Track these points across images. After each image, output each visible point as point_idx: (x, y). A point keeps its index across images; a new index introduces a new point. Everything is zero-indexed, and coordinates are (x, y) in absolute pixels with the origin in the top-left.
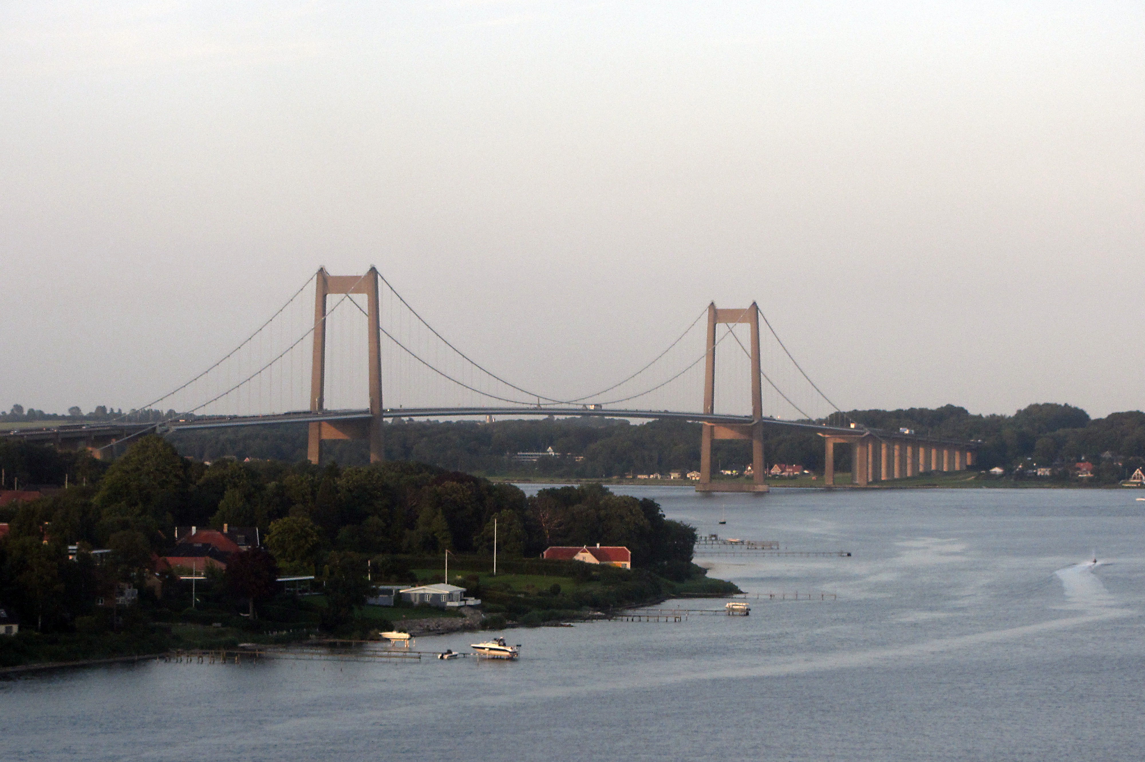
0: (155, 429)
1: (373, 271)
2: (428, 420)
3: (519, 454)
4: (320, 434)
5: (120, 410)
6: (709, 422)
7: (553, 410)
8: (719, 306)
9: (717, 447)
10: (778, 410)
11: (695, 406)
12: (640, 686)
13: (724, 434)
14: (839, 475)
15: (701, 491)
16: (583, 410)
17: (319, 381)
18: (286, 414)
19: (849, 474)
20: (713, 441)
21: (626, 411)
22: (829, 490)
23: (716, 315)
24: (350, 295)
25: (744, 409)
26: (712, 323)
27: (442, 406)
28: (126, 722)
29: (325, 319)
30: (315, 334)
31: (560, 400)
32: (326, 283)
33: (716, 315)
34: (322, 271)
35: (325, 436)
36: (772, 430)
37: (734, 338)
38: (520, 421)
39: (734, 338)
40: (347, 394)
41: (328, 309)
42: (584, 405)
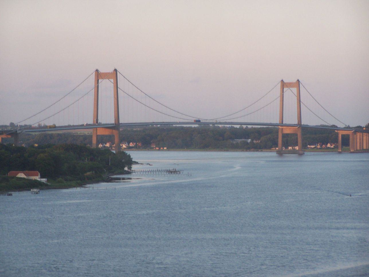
0: (17, 131)
1: (116, 70)
2: (252, 127)
3: (235, 140)
4: (97, 133)
5: (44, 124)
6: (281, 127)
7: (209, 122)
8: (285, 81)
9: (285, 136)
10: (310, 121)
11: (276, 120)
12: (253, 235)
13: (287, 131)
14: (344, 147)
15: (278, 154)
16: (215, 122)
17: (96, 113)
18: (81, 125)
19: (348, 147)
20: (283, 134)
21: (232, 122)
22: (340, 153)
23: (284, 85)
24: (110, 80)
25: (111, 120)
26: (282, 88)
27: (157, 122)
28: (242, 232)
29: (283, 94)
30: (280, 98)
31: (206, 119)
32: (99, 75)
33: (284, 85)
34: (97, 71)
35: (98, 134)
36: (306, 130)
37: (290, 94)
38: (263, 127)
39: (290, 94)
40: (107, 117)
41: (284, 91)
42: (216, 121)
